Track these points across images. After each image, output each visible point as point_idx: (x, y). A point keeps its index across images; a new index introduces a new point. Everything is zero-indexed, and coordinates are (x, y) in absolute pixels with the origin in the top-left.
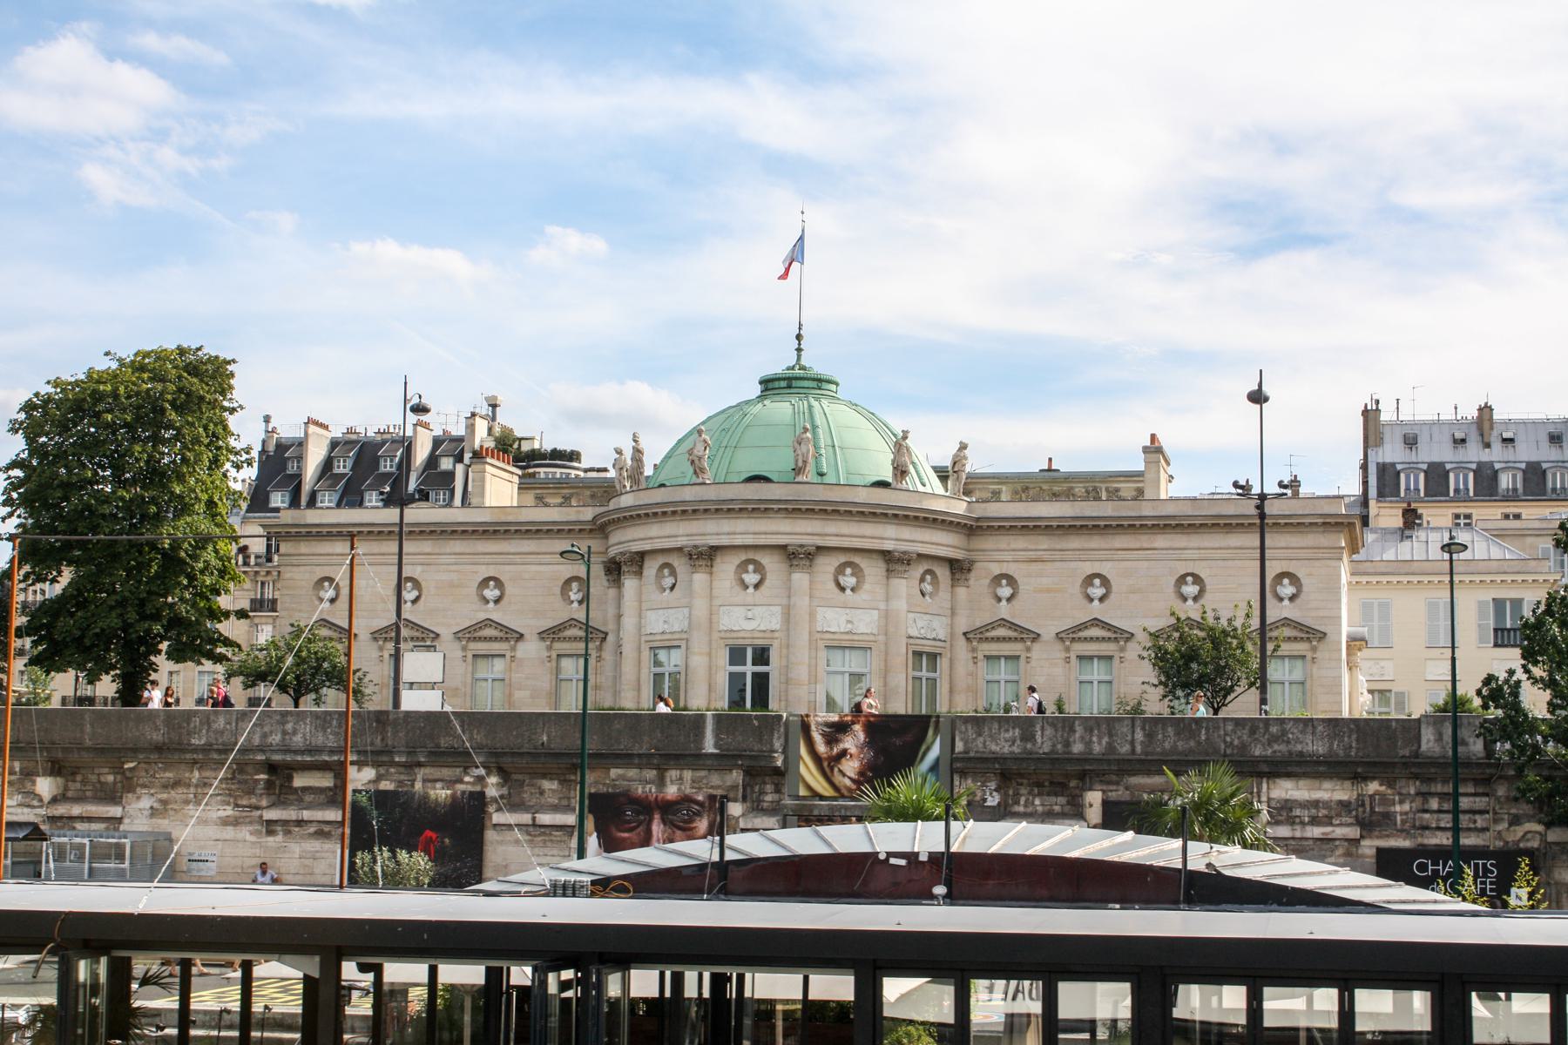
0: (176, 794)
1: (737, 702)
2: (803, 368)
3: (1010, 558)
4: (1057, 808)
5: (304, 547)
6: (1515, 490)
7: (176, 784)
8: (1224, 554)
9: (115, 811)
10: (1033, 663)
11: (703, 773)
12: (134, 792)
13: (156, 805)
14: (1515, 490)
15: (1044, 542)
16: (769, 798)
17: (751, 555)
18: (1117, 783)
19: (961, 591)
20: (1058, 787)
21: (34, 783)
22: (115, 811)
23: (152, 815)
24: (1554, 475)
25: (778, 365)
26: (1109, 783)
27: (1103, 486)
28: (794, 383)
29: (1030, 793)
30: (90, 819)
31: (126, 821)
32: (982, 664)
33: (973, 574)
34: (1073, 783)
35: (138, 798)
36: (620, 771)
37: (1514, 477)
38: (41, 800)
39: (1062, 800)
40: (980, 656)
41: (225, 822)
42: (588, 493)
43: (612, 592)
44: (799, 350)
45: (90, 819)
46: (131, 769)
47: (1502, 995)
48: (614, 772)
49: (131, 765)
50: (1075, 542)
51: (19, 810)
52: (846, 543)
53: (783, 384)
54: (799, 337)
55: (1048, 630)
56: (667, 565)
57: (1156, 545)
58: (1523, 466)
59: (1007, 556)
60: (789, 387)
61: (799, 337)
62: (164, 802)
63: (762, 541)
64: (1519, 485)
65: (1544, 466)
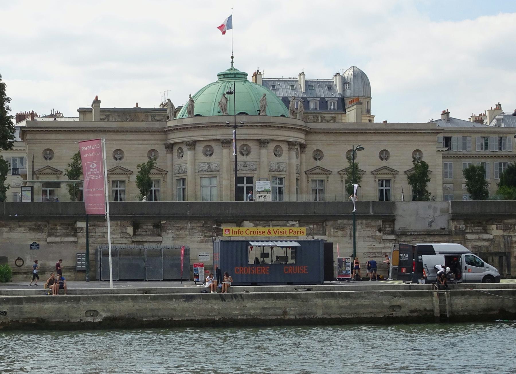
0: (182, 232)
1: (381, 198)
2: (235, 70)
3: (320, 144)
4: (479, 231)
5: (38, 136)
6: (316, 109)
7: (182, 228)
8: (396, 143)
9: (160, 239)
10: (329, 182)
11: (369, 221)
12: (166, 232)
13: (174, 236)
14: (316, 109)
15: (333, 138)
16: (387, 229)
17: (245, 142)
18: (501, 222)
19: (303, 156)
20: (479, 224)
21: (126, 229)
22: (160, 239)
23: (173, 240)
24: (331, 103)
25: (225, 68)
26: (498, 222)
27: (319, 115)
28: (237, 76)
29: (471, 226)
30: (150, 242)
31: (163, 242)
32: (311, 183)
33: (306, 149)
34: (484, 223)
35: (168, 234)
36: (341, 221)
37: (316, 103)
38: (130, 235)
39: (481, 228)
40: (310, 180)
41: (201, 242)
42: (116, 114)
43: (169, 156)
44: (232, 62)
45: (150, 242)
46: (164, 224)
47: (298, 317)
48: (339, 222)
49: (164, 222)
50: (344, 138)
51: (121, 239)
52: (279, 139)
53: (233, 76)
54: (232, 57)
55: (335, 170)
56: (208, 146)
57: (373, 139)
58: (319, 99)
59: (319, 143)
60: (235, 77)
61: (232, 57)
62: (178, 235)
63: (252, 138)
64: (318, 107)
65: (327, 99)
